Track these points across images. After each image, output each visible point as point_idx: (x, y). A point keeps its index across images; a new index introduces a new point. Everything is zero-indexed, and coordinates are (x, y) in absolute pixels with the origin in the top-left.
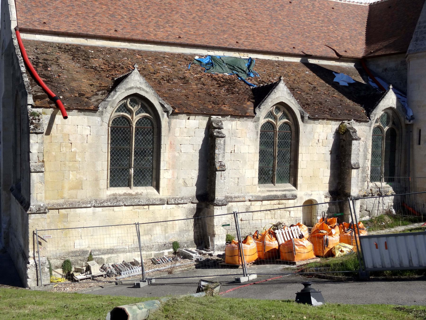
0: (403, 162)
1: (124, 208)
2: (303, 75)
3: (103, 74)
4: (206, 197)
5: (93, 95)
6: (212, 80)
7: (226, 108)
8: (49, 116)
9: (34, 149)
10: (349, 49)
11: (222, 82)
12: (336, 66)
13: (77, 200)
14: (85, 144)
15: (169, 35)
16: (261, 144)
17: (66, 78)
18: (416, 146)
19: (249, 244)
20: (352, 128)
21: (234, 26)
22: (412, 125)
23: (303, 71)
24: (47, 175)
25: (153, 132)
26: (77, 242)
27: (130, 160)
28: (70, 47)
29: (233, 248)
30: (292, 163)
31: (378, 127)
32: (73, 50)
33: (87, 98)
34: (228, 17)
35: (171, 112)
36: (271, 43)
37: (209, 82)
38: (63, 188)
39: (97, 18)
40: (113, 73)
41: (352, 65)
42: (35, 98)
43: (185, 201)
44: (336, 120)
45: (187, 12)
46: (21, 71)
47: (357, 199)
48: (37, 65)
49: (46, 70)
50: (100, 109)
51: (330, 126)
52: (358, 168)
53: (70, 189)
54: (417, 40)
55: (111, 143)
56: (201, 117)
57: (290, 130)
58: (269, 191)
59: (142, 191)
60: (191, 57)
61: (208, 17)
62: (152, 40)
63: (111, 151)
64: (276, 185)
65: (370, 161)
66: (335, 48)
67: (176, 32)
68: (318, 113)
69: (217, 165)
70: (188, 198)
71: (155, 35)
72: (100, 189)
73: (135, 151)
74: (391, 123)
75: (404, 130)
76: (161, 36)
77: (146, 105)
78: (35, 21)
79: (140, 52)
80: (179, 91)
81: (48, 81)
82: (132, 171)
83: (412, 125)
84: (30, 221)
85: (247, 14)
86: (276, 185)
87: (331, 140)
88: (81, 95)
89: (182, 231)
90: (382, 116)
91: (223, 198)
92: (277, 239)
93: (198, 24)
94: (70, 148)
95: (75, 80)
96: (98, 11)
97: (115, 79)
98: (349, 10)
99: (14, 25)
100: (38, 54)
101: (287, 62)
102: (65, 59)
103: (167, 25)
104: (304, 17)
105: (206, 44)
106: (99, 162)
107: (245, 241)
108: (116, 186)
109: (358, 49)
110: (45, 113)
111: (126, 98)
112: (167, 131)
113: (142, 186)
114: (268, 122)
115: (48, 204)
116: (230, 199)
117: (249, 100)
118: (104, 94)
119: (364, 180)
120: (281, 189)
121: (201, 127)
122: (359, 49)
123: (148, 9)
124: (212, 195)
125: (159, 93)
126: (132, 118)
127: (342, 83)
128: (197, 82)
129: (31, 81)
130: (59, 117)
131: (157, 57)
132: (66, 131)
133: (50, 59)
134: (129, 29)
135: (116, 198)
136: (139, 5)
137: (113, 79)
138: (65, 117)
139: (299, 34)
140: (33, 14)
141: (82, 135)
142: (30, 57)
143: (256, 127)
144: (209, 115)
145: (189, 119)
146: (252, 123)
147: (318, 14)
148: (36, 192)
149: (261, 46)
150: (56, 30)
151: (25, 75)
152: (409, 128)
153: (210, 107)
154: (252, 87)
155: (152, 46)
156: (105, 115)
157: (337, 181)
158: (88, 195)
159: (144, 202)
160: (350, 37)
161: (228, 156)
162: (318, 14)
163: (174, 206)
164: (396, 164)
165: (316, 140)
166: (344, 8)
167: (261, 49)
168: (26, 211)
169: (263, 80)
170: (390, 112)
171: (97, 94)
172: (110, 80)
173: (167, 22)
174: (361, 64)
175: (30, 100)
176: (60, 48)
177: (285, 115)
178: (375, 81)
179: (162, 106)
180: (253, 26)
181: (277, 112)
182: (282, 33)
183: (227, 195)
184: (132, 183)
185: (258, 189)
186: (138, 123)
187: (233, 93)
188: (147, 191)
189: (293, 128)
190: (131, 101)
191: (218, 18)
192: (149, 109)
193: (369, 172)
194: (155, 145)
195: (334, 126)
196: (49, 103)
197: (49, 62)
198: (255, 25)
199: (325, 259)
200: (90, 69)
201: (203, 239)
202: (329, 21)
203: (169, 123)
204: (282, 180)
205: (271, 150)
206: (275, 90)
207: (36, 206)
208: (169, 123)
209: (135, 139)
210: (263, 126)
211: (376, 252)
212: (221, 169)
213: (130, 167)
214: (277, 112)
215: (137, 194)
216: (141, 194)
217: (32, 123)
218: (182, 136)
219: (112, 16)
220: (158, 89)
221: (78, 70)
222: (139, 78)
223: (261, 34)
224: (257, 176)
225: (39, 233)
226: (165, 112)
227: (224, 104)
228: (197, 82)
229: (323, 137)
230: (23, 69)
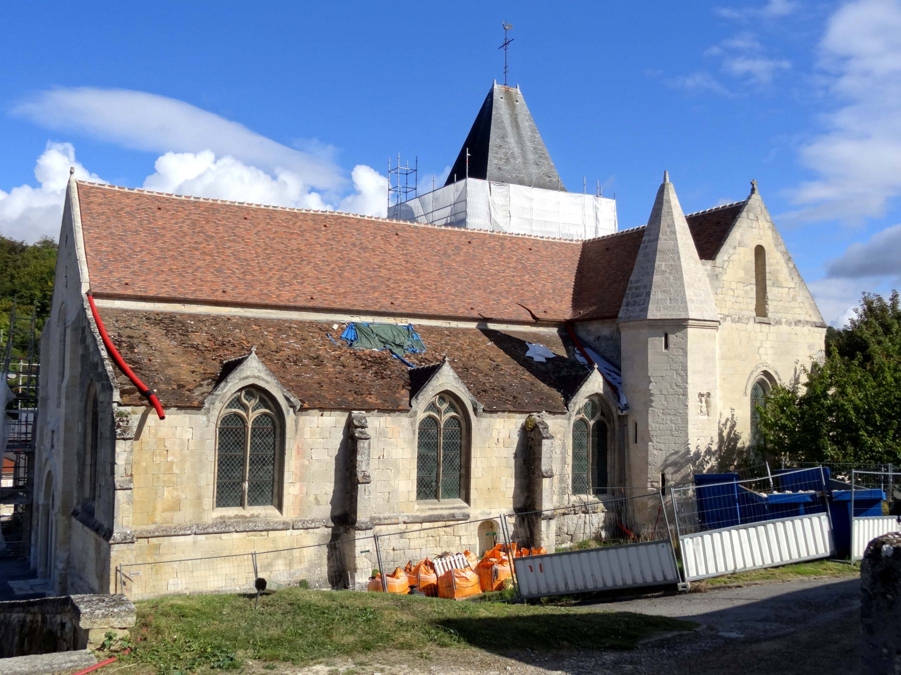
0: (617, 466)
1: (235, 535)
2: (483, 347)
3: (209, 355)
4: (344, 519)
5: (196, 387)
6: (355, 360)
7: (372, 400)
8: (140, 416)
9: (121, 460)
10: (550, 308)
11: (370, 361)
12: (531, 333)
13: (173, 525)
14: (186, 452)
15: (298, 295)
16: (420, 446)
17: (159, 363)
18: (632, 445)
19: (398, 578)
20: (543, 423)
21: (389, 279)
22: (626, 416)
23: (484, 343)
24: (136, 494)
25: (274, 433)
26: (171, 581)
27: (244, 471)
28: (161, 316)
29: (378, 583)
30: (463, 471)
31: (582, 420)
32: (166, 321)
33: (189, 390)
34: (380, 267)
35: (298, 408)
36: (440, 303)
37: (351, 362)
38: (154, 508)
39: (199, 274)
40: (221, 353)
41: (554, 330)
42: (123, 393)
43: (317, 524)
44: (522, 412)
45: (324, 261)
46: (101, 356)
47: (550, 518)
48: (119, 345)
49: (132, 352)
50: (206, 405)
51: (513, 420)
52: (551, 476)
53: (164, 511)
54: (627, 305)
55: (219, 449)
56: (338, 413)
57: (460, 426)
58: (432, 509)
59: (260, 511)
60: (327, 326)
61: (353, 268)
62: (274, 303)
63: (219, 460)
64: (442, 500)
65: (570, 466)
66: (531, 307)
67: (307, 290)
68: (497, 401)
69: (360, 476)
70: (321, 520)
71: (278, 296)
72: (204, 510)
73: (251, 459)
74: (598, 414)
75: (617, 423)
76: (286, 297)
77: (266, 399)
78: (114, 282)
79: (256, 321)
80: (309, 377)
81: (136, 368)
82: (246, 485)
83: (626, 416)
84: (113, 554)
85: (407, 262)
86: (442, 500)
87: (515, 439)
88: (181, 386)
89: (312, 566)
90: (586, 406)
91: (368, 519)
92: (435, 572)
93: (338, 279)
94: (166, 458)
95: (171, 366)
96: (199, 263)
97: (225, 362)
98: (553, 251)
99: (85, 288)
100: (120, 329)
101: (462, 329)
102: (155, 335)
103: (295, 281)
104: (489, 264)
105: (348, 307)
106: (204, 475)
107: (394, 575)
108: (224, 506)
109: (564, 307)
110: (134, 413)
111: (240, 390)
112: (294, 433)
113: (260, 505)
114: (430, 417)
115: (135, 531)
116: (377, 521)
117: (403, 387)
118: (211, 384)
119: (563, 492)
120: (447, 506)
121: (338, 426)
122: (564, 310)
123: (269, 259)
124: (353, 516)
125: (285, 383)
126: (248, 416)
127: (537, 359)
128: (334, 363)
129: (114, 368)
130: (153, 417)
131: (280, 327)
132: (161, 434)
133: (135, 335)
134: (242, 288)
135: (224, 522)
136: (256, 253)
137: (221, 362)
138: (162, 418)
139: (480, 288)
140: (111, 272)
141: (181, 440)
142: (111, 334)
143: (412, 424)
144: (349, 410)
145: (322, 415)
146: (407, 419)
147: (509, 258)
148: (121, 515)
149: (425, 308)
150: (143, 294)
151: (107, 362)
152: (623, 420)
153: (351, 399)
154: (409, 368)
155: (274, 311)
156: (212, 412)
157: (526, 494)
158: (187, 519)
159: (261, 526)
160: (554, 291)
161: (374, 463)
162: (509, 258)
163: (302, 531)
164: (608, 470)
165: (495, 441)
166: (547, 248)
167: (425, 312)
168: (108, 540)
169: (427, 356)
170: (596, 399)
171: (201, 385)
172: (217, 363)
173: (294, 278)
174: (568, 329)
175: (116, 396)
176: (148, 319)
177: (452, 407)
178: (584, 354)
179: (288, 399)
180: (415, 279)
181: (441, 404)
182: (455, 287)
183: (374, 515)
184: (246, 501)
185: (417, 507)
186: (256, 421)
187: (383, 378)
188: (265, 512)
189: (463, 424)
190: (246, 394)
191: (367, 269)
192: (270, 403)
193: (570, 481)
194: (277, 450)
195: (518, 420)
196: (140, 399)
197: (135, 341)
198: (418, 277)
199: (45, 405)
200: (190, 349)
201: (340, 575)
202: (525, 268)
203: (297, 422)
204: (449, 494)
205: (434, 454)
206: (438, 375)
207: (121, 533)
208: (297, 422)
209: (251, 443)
210: (423, 423)
211: (531, 575)
212: (364, 481)
213: (243, 480)
214: (441, 404)
215: (252, 516)
216: (258, 516)
217: (119, 426)
218: (313, 439)
219: (219, 270)
220: (282, 375)
221: (175, 350)
222: (257, 365)
223: (426, 291)
224: (415, 489)
225: (124, 570)
226: (291, 407)
227: (370, 394)
228: (334, 363)
229: (503, 434)
230: (104, 354)
